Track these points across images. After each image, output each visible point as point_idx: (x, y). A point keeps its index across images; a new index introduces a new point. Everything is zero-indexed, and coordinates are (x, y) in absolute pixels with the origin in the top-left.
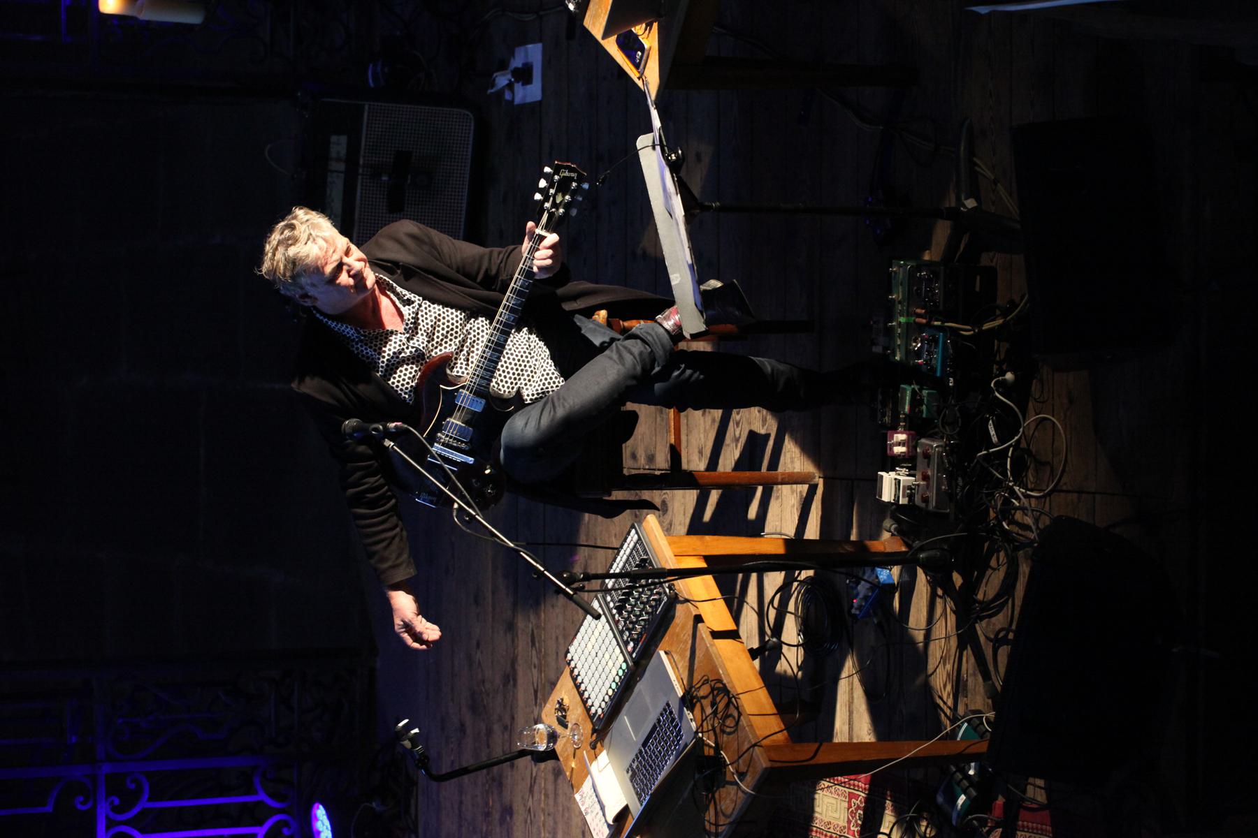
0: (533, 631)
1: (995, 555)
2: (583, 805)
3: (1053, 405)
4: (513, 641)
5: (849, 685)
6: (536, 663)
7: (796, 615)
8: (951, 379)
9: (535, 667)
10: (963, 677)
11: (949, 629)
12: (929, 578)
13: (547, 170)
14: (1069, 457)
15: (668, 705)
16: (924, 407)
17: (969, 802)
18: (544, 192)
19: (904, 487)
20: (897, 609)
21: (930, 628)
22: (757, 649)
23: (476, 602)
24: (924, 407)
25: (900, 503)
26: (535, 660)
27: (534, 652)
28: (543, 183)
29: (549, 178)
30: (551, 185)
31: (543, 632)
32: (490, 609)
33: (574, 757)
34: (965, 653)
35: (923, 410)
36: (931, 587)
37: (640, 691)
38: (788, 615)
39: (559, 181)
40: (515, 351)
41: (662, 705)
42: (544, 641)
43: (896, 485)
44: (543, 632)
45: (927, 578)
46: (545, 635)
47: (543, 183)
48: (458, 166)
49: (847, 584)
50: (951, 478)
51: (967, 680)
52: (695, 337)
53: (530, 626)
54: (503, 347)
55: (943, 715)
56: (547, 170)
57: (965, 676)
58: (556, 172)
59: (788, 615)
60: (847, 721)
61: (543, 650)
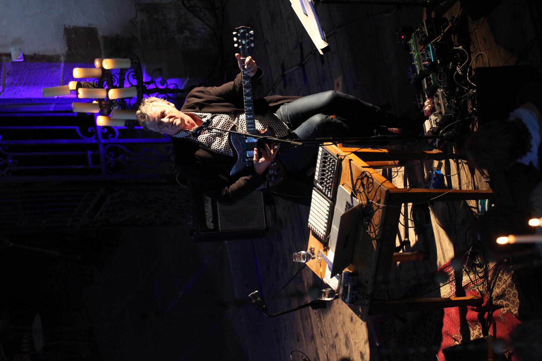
0: (321, 331)
1: (475, 126)
2: (327, 281)
3: (479, 48)
4: (315, 343)
5: (437, 232)
6: (325, 343)
7: (411, 220)
8: (438, 60)
9: (324, 345)
10: (477, 186)
11: (466, 172)
12: (454, 160)
13: (234, 33)
14: (490, 62)
15: (347, 203)
16: (432, 80)
17: (489, 200)
18: (237, 42)
19: (433, 121)
20: (447, 184)
21: (459, 172)
22: (400, 246)
23: (298, 340)
24: (432, 80)
25: (433, 127)
26: (324, 342)
27: (323, 339)
28: (235, 39)
29: (236, 36)
30: (238, 39)
31: (325, 327)
32: (304, 338)
33: (321, 273)
34: (475, 176)
35: (432, 82)
36: (456, 162)
37: (337, 208)
38: (409, 228)
39: (241, 35)
40: (242, 117)
41: (345, 204)
42: (326, 331)
43: (430, 122)
44: (325, 327)
45: (453, 160)
46: (325, 328)
47: (235, 39)
48: (247, 206)
49: (397, 32)
50: (448, 100)
51: (478, 186)
52: (334, 118)
53: (319, 329)
54: (251, 157)
55: (473, 209)
56: (234, 33)
57: (477, 185)
58: (238, 32)
59: (409, 228)
60: (440, 248)
61: (326, 335)
